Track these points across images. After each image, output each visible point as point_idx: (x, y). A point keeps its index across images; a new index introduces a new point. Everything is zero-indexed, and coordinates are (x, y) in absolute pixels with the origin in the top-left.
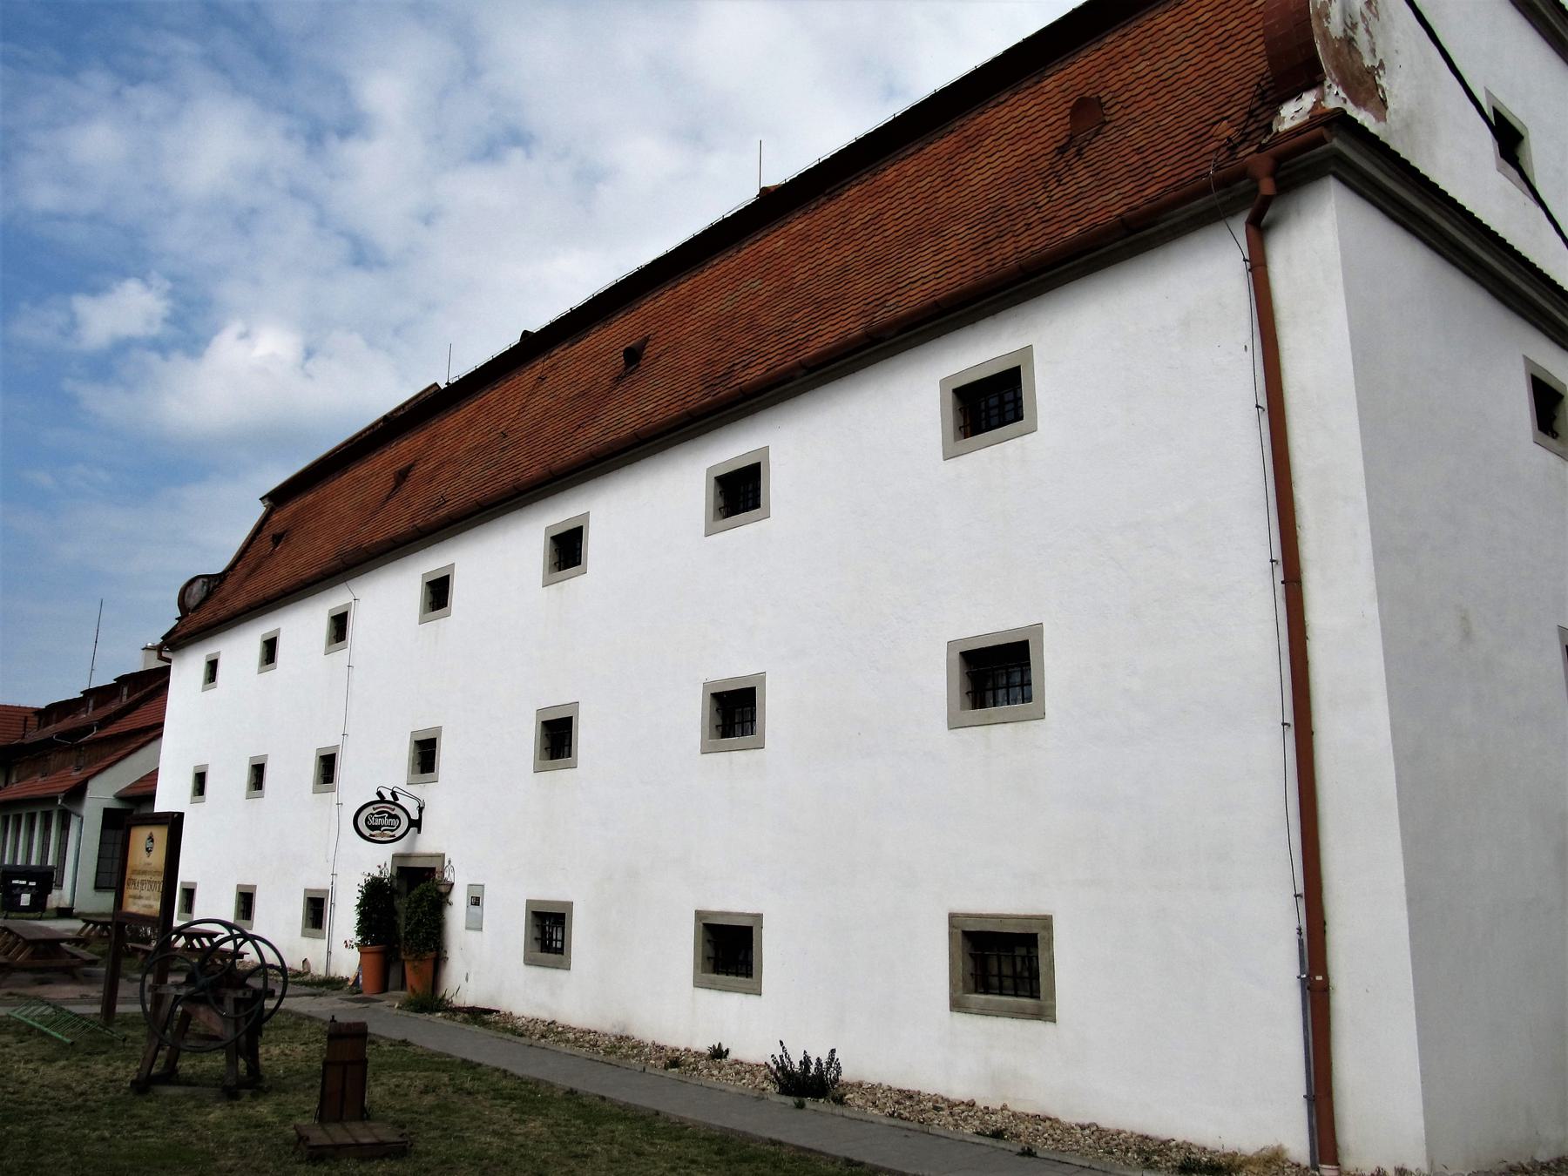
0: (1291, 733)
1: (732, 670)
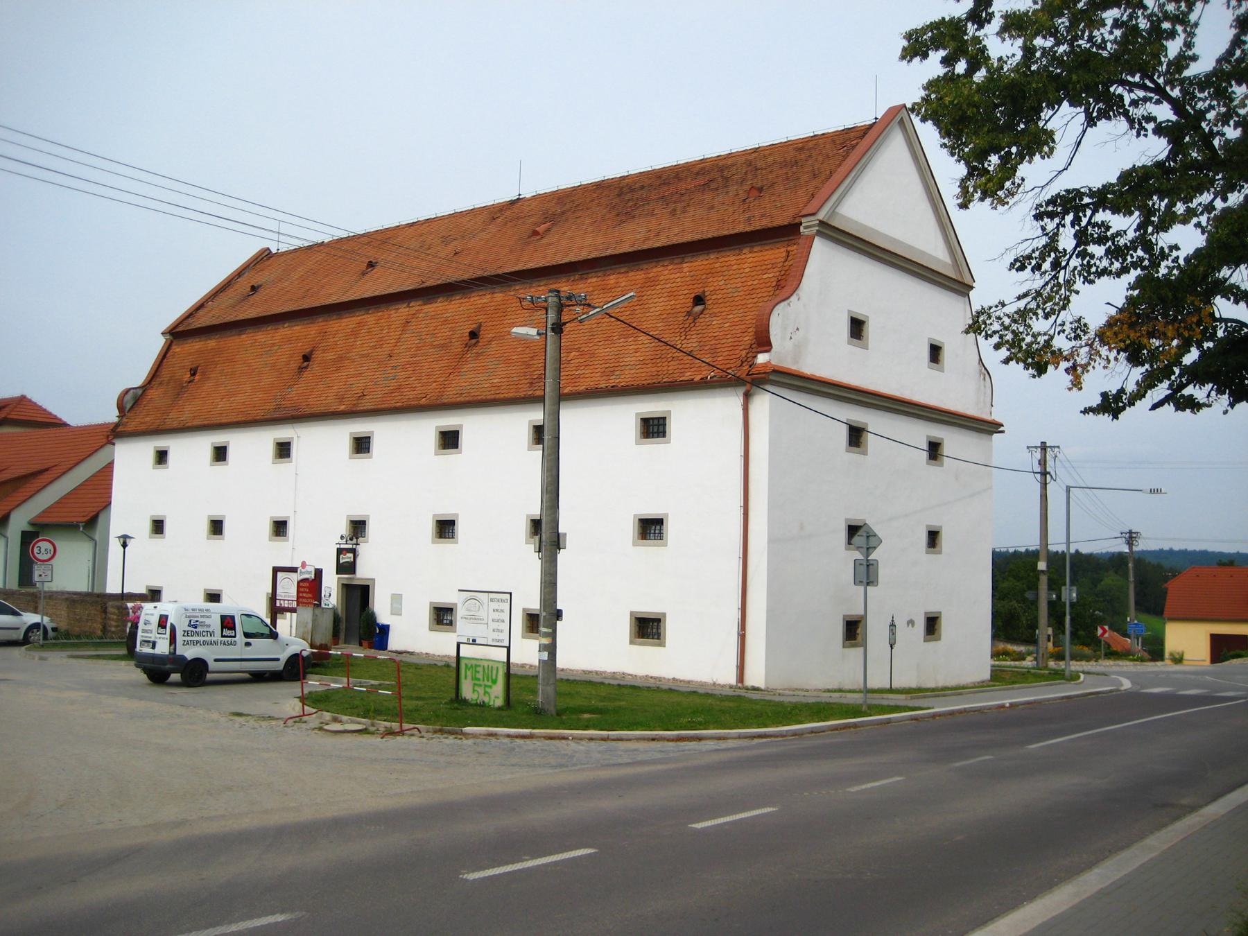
0: (741, 560)
1: (280, 515)
